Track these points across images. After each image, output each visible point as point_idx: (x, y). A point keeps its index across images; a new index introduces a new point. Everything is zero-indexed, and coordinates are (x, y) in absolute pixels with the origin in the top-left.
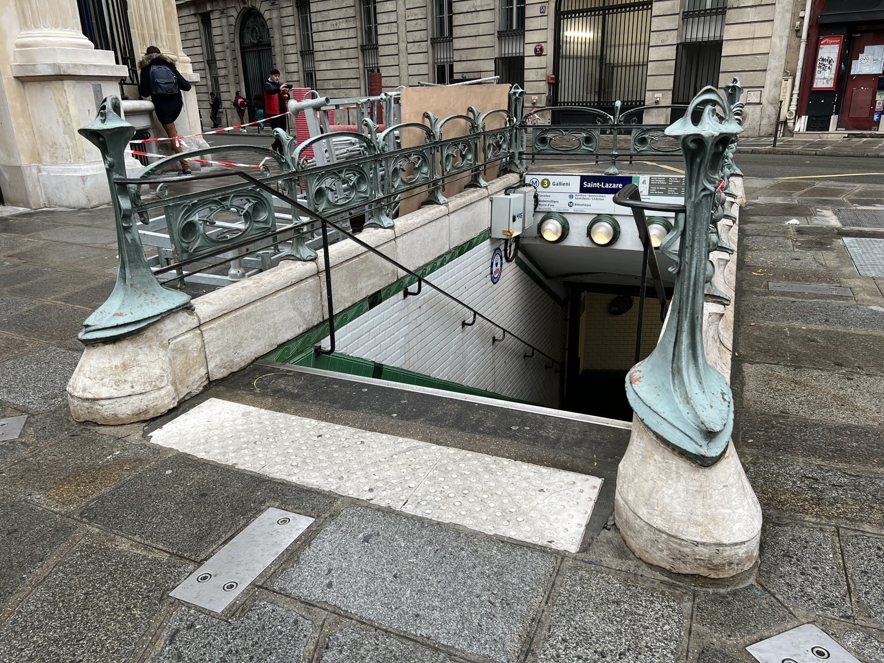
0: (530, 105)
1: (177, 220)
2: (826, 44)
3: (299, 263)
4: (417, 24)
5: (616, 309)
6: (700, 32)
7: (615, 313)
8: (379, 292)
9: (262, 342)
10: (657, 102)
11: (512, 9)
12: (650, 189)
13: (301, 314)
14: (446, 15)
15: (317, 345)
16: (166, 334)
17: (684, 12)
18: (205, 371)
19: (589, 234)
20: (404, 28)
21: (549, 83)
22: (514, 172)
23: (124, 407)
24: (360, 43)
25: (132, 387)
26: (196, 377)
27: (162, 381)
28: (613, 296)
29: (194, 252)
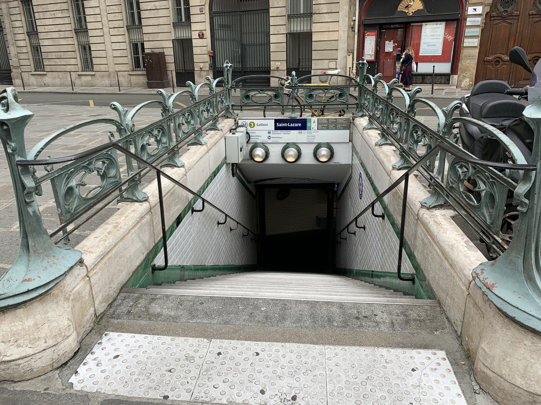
0: (199, 69)
1: (61, 187)
2: (368, 35)
3: (137, 204)
4: (115, 16)
6: (299, 27)
8: (180, 214)
9: (124, 273)
10: (278, 68)
11: (180, 9)
12: (318, 126)
13: (144, 243)
14: (135, 11)
15: (152, 264)
16: (68, 288)
17: (288, 15)
18: (93, 309)
20: (106, 18)
21: (210, 56)
22: (230, 118)
23: (39, 361)
24: (73, 27)
25: (46, 342)
26: (88, 316)
27: (70, 329)
29: (74, 211)
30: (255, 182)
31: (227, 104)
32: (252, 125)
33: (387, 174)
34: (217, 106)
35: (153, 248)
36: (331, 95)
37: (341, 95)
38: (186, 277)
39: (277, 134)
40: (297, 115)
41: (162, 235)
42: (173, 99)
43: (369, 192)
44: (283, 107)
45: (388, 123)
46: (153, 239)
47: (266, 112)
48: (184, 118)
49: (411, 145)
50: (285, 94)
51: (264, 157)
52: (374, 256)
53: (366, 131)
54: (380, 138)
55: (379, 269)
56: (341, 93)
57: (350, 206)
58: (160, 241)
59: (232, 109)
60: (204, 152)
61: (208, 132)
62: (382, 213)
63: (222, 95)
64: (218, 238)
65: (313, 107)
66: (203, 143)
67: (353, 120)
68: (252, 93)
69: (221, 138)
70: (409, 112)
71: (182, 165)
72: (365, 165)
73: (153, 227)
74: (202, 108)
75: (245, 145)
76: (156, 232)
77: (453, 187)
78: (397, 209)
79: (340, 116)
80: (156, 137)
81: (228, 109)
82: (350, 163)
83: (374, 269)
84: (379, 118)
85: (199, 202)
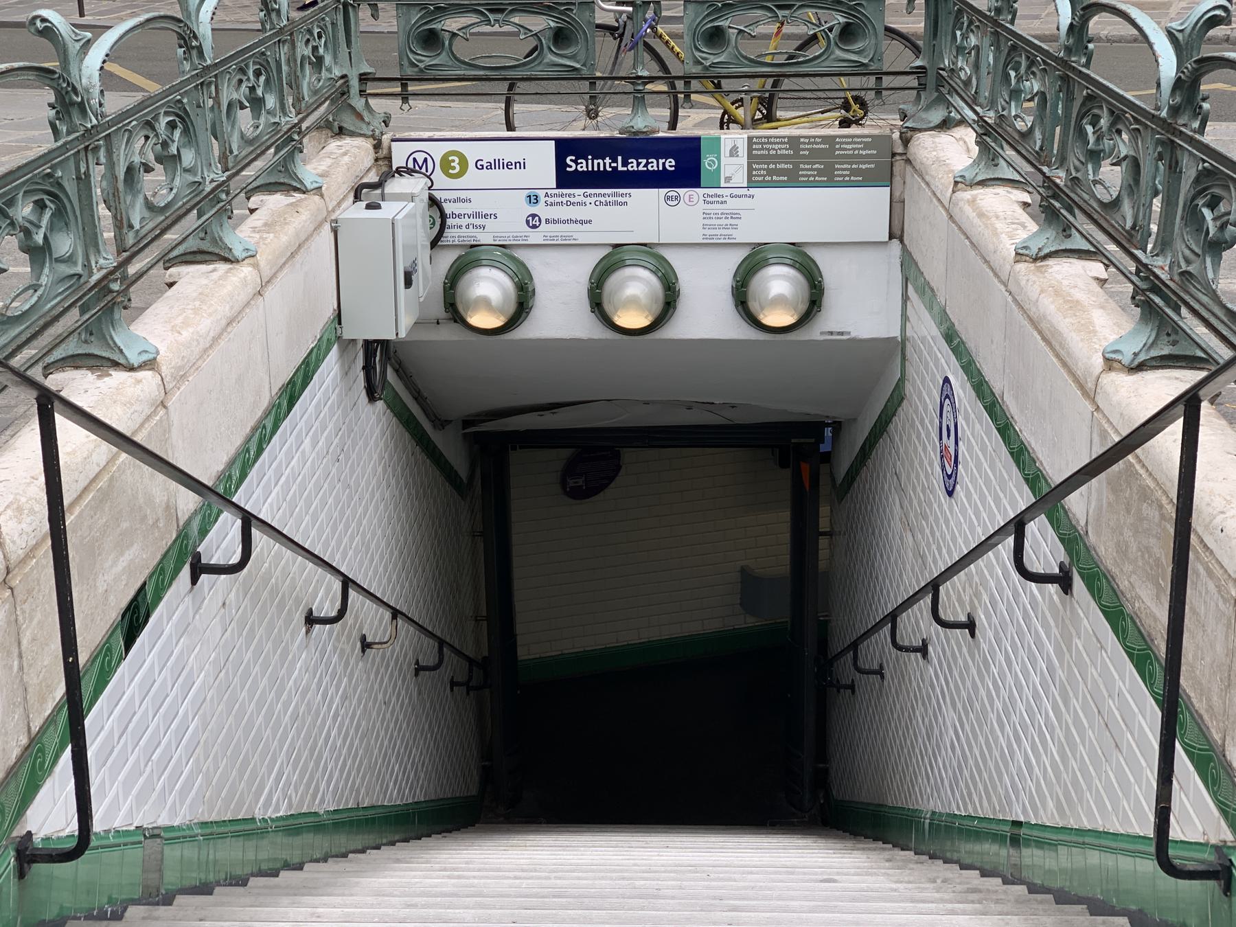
5: (581, 482)
7: (578, 494)
12: (750, 169)
15: (19, 832)
19: (597, 303)
22: (352, 134)
28: (566, 453)
30: (467, 423)
31: (337, 72)
32: (454, 166)
33: (1082, 387)
34: (295, 84)
35: (20, 759)
36: (805, 30)
37: (847, 33)
38: (171, 878)
39: (569, 204)
40: (656, 119)
41: (61, 690)
42: (102, 57)
43: (992, 467)
44: (593, 84)
45: (1073, 161)
46: (19, 711)
47: (517, 108)
48: (151, 142)
49: (1188, 262)
50: (599, 26)
51: (511, 308)
52: (1019, 757)
53: (966, 195)
54: (1033, 227)
55: (1049, 816)
56: (848, 25)
57: (896, 525)
58: (50, 721)
59: (362, 93)
60: (243, 297)
61: (255, 201)
62: (1061, 566)
63: (316, 31)
64: (306, 690)
65: (726, 84)
66: (238, 252)
67: (906, 141)
68: (452, 24)
69: (318, 228)
70: (1175, 111)
71: (145, 357)
72: (971, 345)
73: (20, 656)
74: (229, 93)
75: (424, 254)
76: (32, 679)
78: (1133, 547)
79: (845, 123)
80: (28, 233)
81: (344, 93)
82: (895, 332)
83: (1024, 811)
84: (1027, 135)
85: (227, 529)
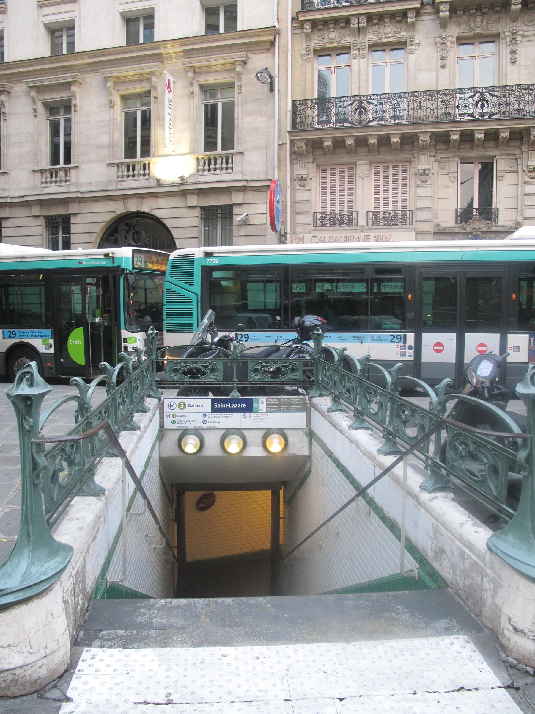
5: (203, 505)
77: (454, 465)
